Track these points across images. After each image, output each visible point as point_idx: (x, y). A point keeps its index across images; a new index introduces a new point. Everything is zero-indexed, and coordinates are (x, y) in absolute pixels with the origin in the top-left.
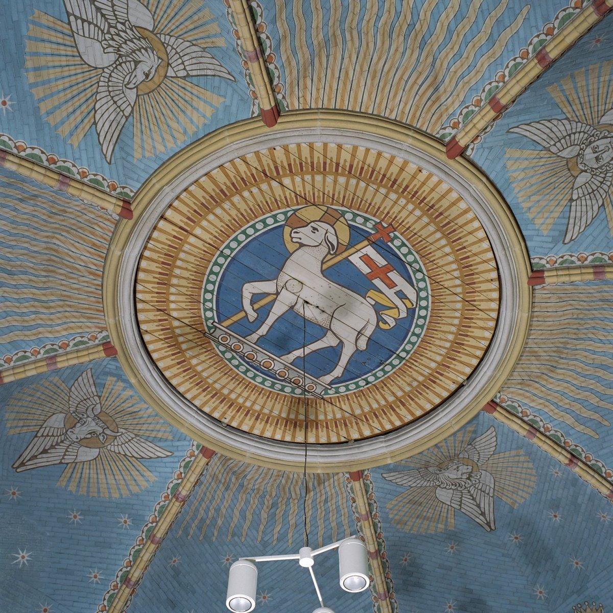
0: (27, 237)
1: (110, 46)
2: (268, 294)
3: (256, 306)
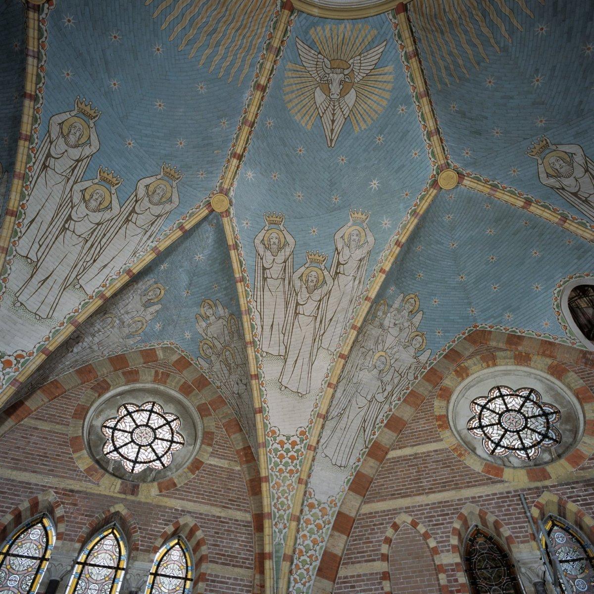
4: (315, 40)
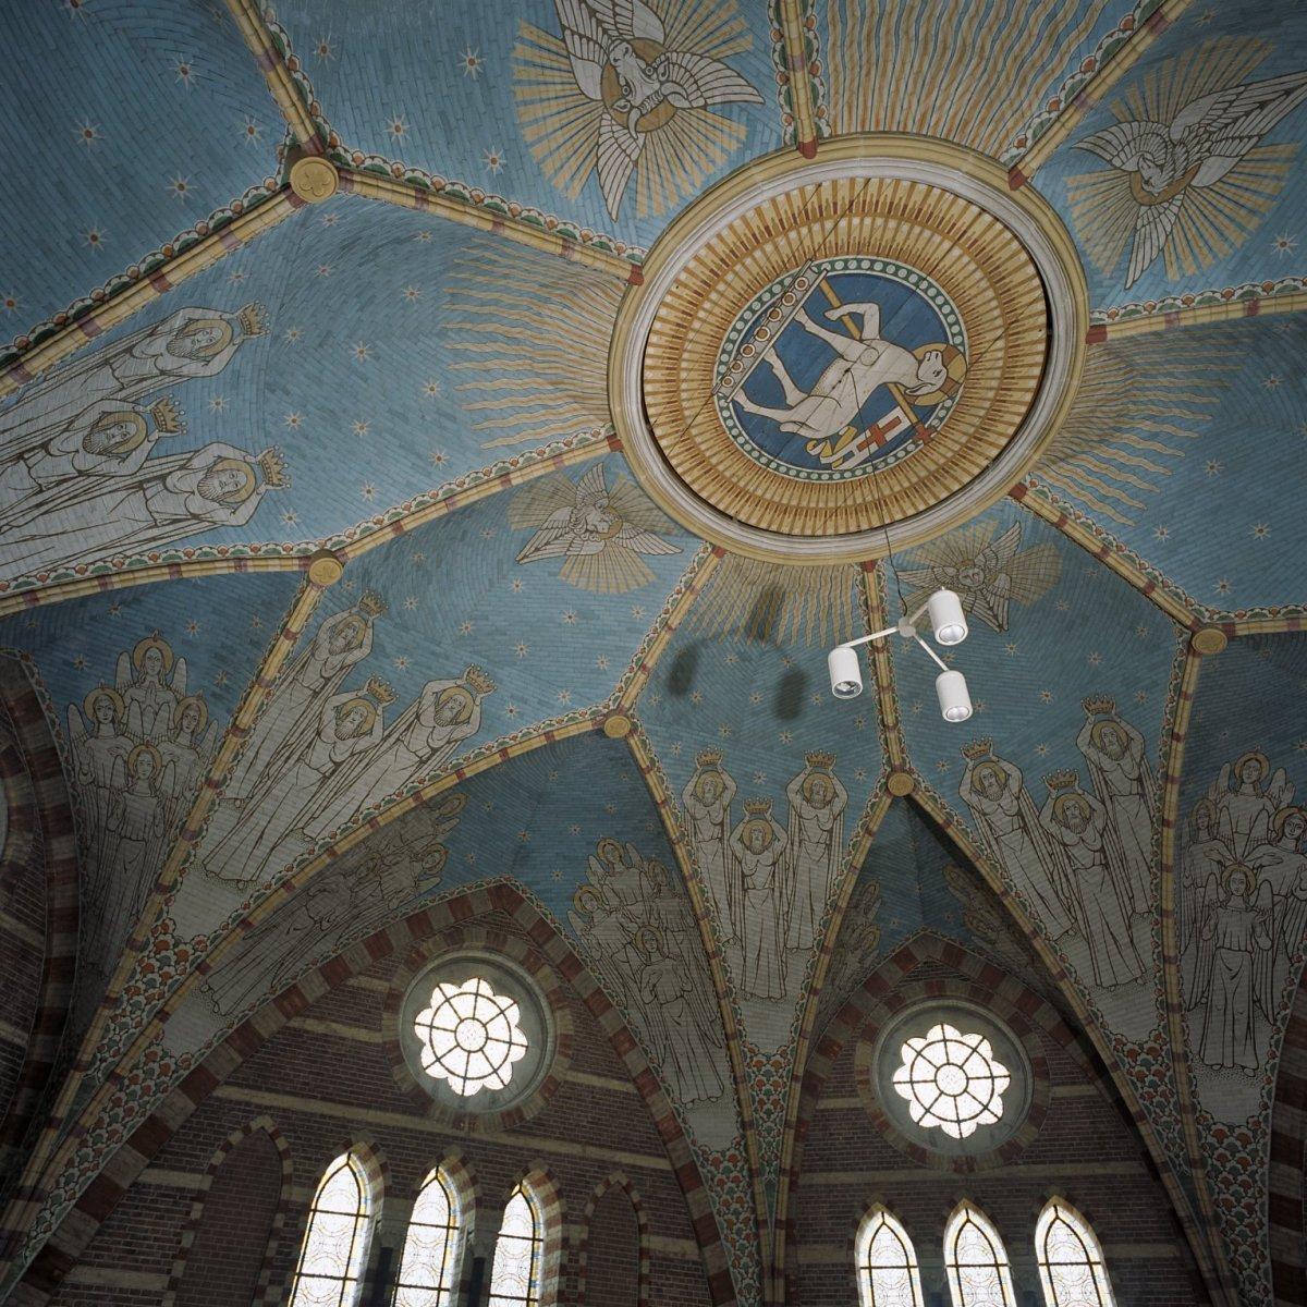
0: (987, 14)
1: (1190, 133)
2: (861, 332)
3: (846, 319)
4: (727, 122)
